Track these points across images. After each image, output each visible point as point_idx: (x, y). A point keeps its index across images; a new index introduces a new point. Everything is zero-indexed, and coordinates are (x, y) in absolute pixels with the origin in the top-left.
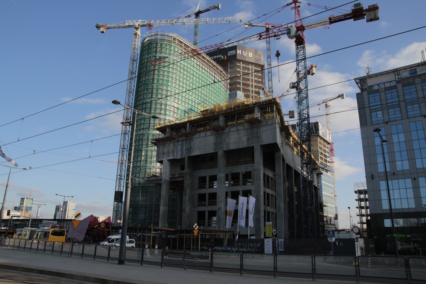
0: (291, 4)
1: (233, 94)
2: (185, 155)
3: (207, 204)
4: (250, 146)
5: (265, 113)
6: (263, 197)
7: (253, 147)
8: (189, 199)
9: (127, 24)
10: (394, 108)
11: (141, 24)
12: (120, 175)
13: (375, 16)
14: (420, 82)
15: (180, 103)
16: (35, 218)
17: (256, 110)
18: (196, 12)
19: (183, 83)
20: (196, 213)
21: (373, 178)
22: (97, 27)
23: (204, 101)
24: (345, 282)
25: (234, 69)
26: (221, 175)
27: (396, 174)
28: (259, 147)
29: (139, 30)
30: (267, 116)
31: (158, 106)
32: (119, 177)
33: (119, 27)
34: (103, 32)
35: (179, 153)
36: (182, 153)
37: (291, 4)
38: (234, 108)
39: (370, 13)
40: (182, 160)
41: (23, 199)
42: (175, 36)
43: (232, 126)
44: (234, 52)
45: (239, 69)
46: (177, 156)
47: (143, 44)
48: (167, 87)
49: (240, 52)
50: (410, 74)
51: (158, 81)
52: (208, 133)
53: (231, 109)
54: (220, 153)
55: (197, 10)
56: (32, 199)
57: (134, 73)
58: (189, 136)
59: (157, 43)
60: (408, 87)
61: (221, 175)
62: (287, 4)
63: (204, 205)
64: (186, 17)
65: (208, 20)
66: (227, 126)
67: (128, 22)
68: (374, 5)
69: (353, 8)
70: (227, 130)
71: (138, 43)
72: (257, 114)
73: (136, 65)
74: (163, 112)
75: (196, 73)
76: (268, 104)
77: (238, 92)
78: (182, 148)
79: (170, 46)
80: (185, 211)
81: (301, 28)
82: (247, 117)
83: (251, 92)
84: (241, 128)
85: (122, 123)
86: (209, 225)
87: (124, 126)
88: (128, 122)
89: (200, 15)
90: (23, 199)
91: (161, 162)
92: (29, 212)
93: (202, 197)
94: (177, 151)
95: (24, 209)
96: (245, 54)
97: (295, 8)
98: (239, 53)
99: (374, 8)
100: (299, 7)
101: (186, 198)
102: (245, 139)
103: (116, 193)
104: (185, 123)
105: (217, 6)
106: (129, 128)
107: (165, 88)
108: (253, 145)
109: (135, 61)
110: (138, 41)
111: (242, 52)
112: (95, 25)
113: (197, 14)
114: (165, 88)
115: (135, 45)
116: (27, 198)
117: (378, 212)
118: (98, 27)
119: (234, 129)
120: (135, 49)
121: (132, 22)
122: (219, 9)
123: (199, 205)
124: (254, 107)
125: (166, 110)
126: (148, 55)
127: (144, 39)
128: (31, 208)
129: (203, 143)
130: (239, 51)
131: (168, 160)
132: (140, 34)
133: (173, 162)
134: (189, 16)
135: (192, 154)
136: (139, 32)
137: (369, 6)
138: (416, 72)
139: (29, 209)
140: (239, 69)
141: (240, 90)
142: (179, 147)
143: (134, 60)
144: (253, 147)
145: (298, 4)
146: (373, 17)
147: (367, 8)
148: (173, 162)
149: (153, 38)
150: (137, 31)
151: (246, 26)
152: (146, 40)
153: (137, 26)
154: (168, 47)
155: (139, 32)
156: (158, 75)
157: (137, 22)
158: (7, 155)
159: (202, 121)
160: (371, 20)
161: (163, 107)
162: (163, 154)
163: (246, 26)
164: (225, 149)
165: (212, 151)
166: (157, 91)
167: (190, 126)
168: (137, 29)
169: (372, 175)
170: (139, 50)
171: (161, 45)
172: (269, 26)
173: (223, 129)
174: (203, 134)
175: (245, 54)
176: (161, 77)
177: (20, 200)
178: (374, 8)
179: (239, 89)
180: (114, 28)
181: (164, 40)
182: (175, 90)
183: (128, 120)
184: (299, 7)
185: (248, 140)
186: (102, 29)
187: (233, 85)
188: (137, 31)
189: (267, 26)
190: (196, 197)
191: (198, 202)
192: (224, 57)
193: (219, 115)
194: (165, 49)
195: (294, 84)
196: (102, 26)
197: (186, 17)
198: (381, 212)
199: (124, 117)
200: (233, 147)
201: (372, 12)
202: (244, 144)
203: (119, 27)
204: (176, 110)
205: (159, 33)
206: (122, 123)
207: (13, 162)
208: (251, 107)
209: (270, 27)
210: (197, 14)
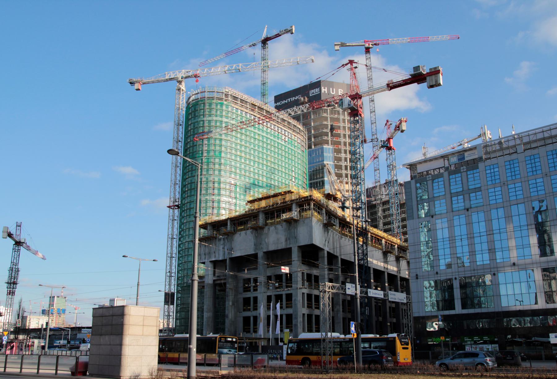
0: (346, 65)
1: (318, 150)
2: (227, 257)
3: (252, 309)
4: (288, 247)
5: (303, 210)
6: (301, 301)
7: (291, 248)
8: (233, 304)
9: (167, 77)
10: (440, 200)
11: (184, 76)
12: (169, 272)
13: (436, 81)
14: (465, 170)
15: (238, 177)
16: (74, 326)
17: (294, 206)
18: (263, 39)
19: (241, 151)
20: (242, 319)
21: (417, 278)
22: (131, 83)
23: (271, 170)
24: (320, 376)
25: (319, 114)
26: (262, 279)
27: (439, 272)
28: (296, 248)
29: (183, 83)
30: (304, 214)
31: (211, 185)
32: (168, 274)
33: (159, 82)
34: (138, 90)
35: (221, 253)
36: (224, 254)
37: (346, 65)
38: (273, 205)
39: (431, 77)
40: (224, 261)
41: (52, 298)
42: (227, 90)
43: (272, 224)
44: (317, 90)
45: (325, 115)
46: (219, 257)
47: (188, 104)
48: (220, 159)
49: (326, 90)
50: (459, 160)
51: (208, 152)
52: (249, 232)
53: (270, 206)
54: (260, 255)
55: (264, 36)
56: (65, 298)
57: (180, 141)
58: (230, 235)
59: (204, 103)
60: (454, 176)
61: (262, 279)
62: (343, 65)
63: (249, 310)
64: (250, 46)
65: (269, 63)
66: (266, 224)
67: (168, 74)
68: (435, 68)
69: (413, 73)
70: (266, 229)
71: (182, 101)
72: (294, 214)
73: (182, 130)
74: (216, 191)
75: (259, 135)
76: (305, 200)
77: (325, 146)
78: (223, 248)
79: (222, 105)
80: (227, 317)
81: (356, 97)
82: (285, 216)
83: (342, 144)
84: (279, 227)
85: (169, 207)
86: (255, 331)
87: (171, 210)
88: (176, 206)
89: (268, 42)
90: (52, 298)
91: (204, 263)
92: (62, 316)
93: (247, 301)
94: (220, 252)
95: (55, 312)
96: (333, 92)
97: (351, 69)
98: (325, 91)
99: (435, 72)
100: (356, 67)
101: (229, 303)
102: (283, 239)
103: (166, 294)
104: (226, 220)
105: (289, 29)
106: (177, 212)
107: (217, 160)
108: (291, 246)
109: (181, 125)
110: (183, 98)
111: (329, 90)
112: (128, 81)
113: (265, 42)
114: (217, 160)
115: (179, 104)
116: (58, 297)
117: (497, 310)
118: (132, 83)
119: (272, 228)
120: (179, 109)
121: (174, 73)
122: (292, 33)
123: (244, 310)
124: (292, 204)
125: (219, 189)
126: (194, 119)
127: (189, 98)
128: (64, 311)
129: (243, 244)
130: (325, 89)
131: (210, 262)
132: (184, 89)
133: (216, 264)
134: (254, 45)
135: (233, 256)
136: (183, 87)
137: (430, 69)
138: (464, 158)
139: (62, 312)
140: (325, 115)
141: (328, 143)
142: (221, 247)
143: (179, 125)
144: (291, 248)
145: (354, 65)
146: (434, 83)
147: (428, 71)
148: (216, 264)
149: (199, 96)
150: (181, 86)
151: (337, 48)
152: (191, 100)
153: (180, 79)
154: (219, 107)
155: (183, 87)
156: (209, 145)
157: (180, 72)
158: (32, 247)
159: (242, 218)
160: (431, 87)
161: (216, 185)
162: (205, 254)
163: (337, 48)
164: (265, 250)
165: (251, 252)
166: (208, 165)
167: (231, 224)
168: (180, 82)
169: (417, 275)
170: (184, 109)
171: (210, 104)
172: (369, 44)
173: (262, 228)
174: (243, 233)
175: (333, 92)
176: (212, 148)
177: (48, 299)
178: (435, 72)
179: (327, 142)
180: (153, 82)
181: (213, 98)
182: (230, 161)
183: (176, 202)
184: (356, 67)
185: (286, 240)
186: (137, 86)
187: (318, 137)
188: (181, 86)
189: (367, 45)
190: (241, 301)
191: (244, 306)
192: (304, 99)
193: (258, 212)
194: (215, 110)
195: (384, 142)
196: (137, 82)
197: (250, 46)
198: (500, 310)
199: (170, 198)
200: (272, 248)
201: (433, 76)
202: (282, 245)
203: (159, 82)
204: (233, 188)
205: (206, 90)
206: (169, 207)
207: (40, 255)
208: (289, 205)
209: (371, 46)
210: (265, 42)
